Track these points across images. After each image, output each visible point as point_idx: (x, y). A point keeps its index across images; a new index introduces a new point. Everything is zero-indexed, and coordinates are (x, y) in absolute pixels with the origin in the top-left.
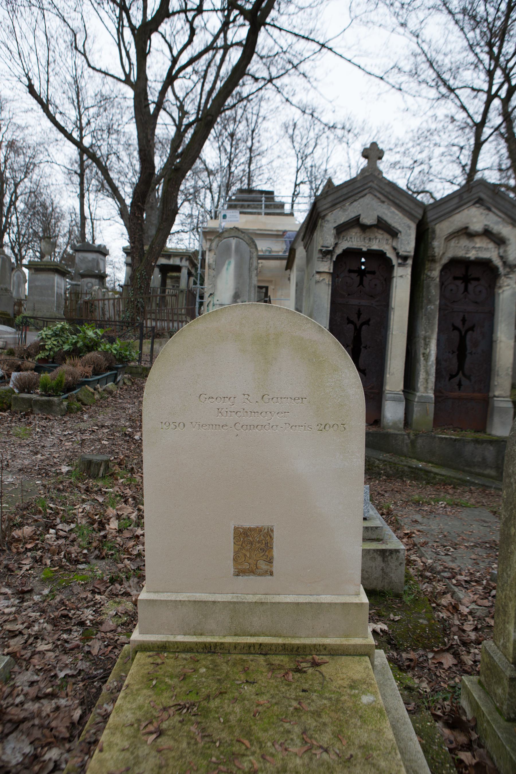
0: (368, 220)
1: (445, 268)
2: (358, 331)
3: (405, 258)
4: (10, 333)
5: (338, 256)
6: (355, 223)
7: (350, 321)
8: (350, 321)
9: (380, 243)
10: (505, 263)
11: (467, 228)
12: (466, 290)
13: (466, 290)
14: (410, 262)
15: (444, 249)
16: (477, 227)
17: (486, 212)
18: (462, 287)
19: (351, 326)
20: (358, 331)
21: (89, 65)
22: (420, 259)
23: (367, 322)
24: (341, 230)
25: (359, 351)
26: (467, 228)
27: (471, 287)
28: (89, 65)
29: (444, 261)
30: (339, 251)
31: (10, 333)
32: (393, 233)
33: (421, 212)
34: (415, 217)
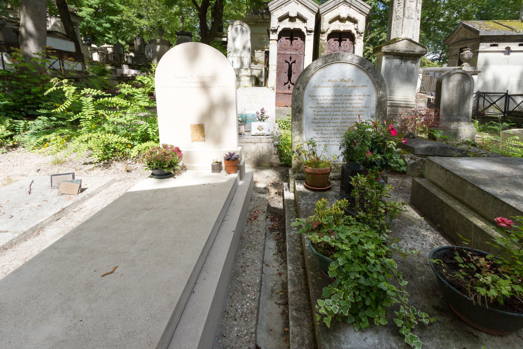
0: (293, 14)
1: (330, 37)
2: (290, 67)
3: (310, 32)
4: (466, 165)
5: (280, 32)
6: (286, 16)
7: (286, 62)
8: (286, 62)
9: (298, 25)
10: (357, 32)
11: (339, 16)
12: (340, 45)
13: (340, 45)
14: (313, 34)
15: (327, 27)
16: (344, 15)
17: (349, 8)
18: (338, 44)
19: (287, 64)
20: (290, 67)
21: (112, 272)
22: (317, 31)
23: (294, 62)
24: (281, 19)
25: (291, 75)
26: (339, 16)
27: (342, 44)
28: (112, 272)
29: (329, 32)
30: (280, 30)
31: (466, 165)
32: (304, 20)
33: (317, 9)
34: (315, 12)
